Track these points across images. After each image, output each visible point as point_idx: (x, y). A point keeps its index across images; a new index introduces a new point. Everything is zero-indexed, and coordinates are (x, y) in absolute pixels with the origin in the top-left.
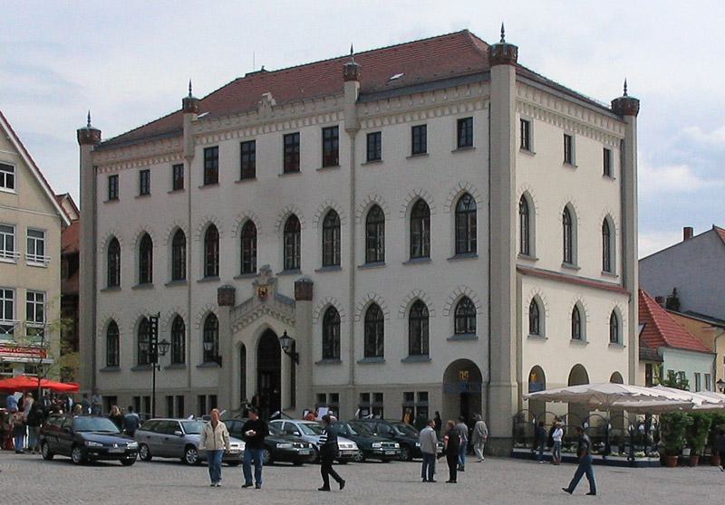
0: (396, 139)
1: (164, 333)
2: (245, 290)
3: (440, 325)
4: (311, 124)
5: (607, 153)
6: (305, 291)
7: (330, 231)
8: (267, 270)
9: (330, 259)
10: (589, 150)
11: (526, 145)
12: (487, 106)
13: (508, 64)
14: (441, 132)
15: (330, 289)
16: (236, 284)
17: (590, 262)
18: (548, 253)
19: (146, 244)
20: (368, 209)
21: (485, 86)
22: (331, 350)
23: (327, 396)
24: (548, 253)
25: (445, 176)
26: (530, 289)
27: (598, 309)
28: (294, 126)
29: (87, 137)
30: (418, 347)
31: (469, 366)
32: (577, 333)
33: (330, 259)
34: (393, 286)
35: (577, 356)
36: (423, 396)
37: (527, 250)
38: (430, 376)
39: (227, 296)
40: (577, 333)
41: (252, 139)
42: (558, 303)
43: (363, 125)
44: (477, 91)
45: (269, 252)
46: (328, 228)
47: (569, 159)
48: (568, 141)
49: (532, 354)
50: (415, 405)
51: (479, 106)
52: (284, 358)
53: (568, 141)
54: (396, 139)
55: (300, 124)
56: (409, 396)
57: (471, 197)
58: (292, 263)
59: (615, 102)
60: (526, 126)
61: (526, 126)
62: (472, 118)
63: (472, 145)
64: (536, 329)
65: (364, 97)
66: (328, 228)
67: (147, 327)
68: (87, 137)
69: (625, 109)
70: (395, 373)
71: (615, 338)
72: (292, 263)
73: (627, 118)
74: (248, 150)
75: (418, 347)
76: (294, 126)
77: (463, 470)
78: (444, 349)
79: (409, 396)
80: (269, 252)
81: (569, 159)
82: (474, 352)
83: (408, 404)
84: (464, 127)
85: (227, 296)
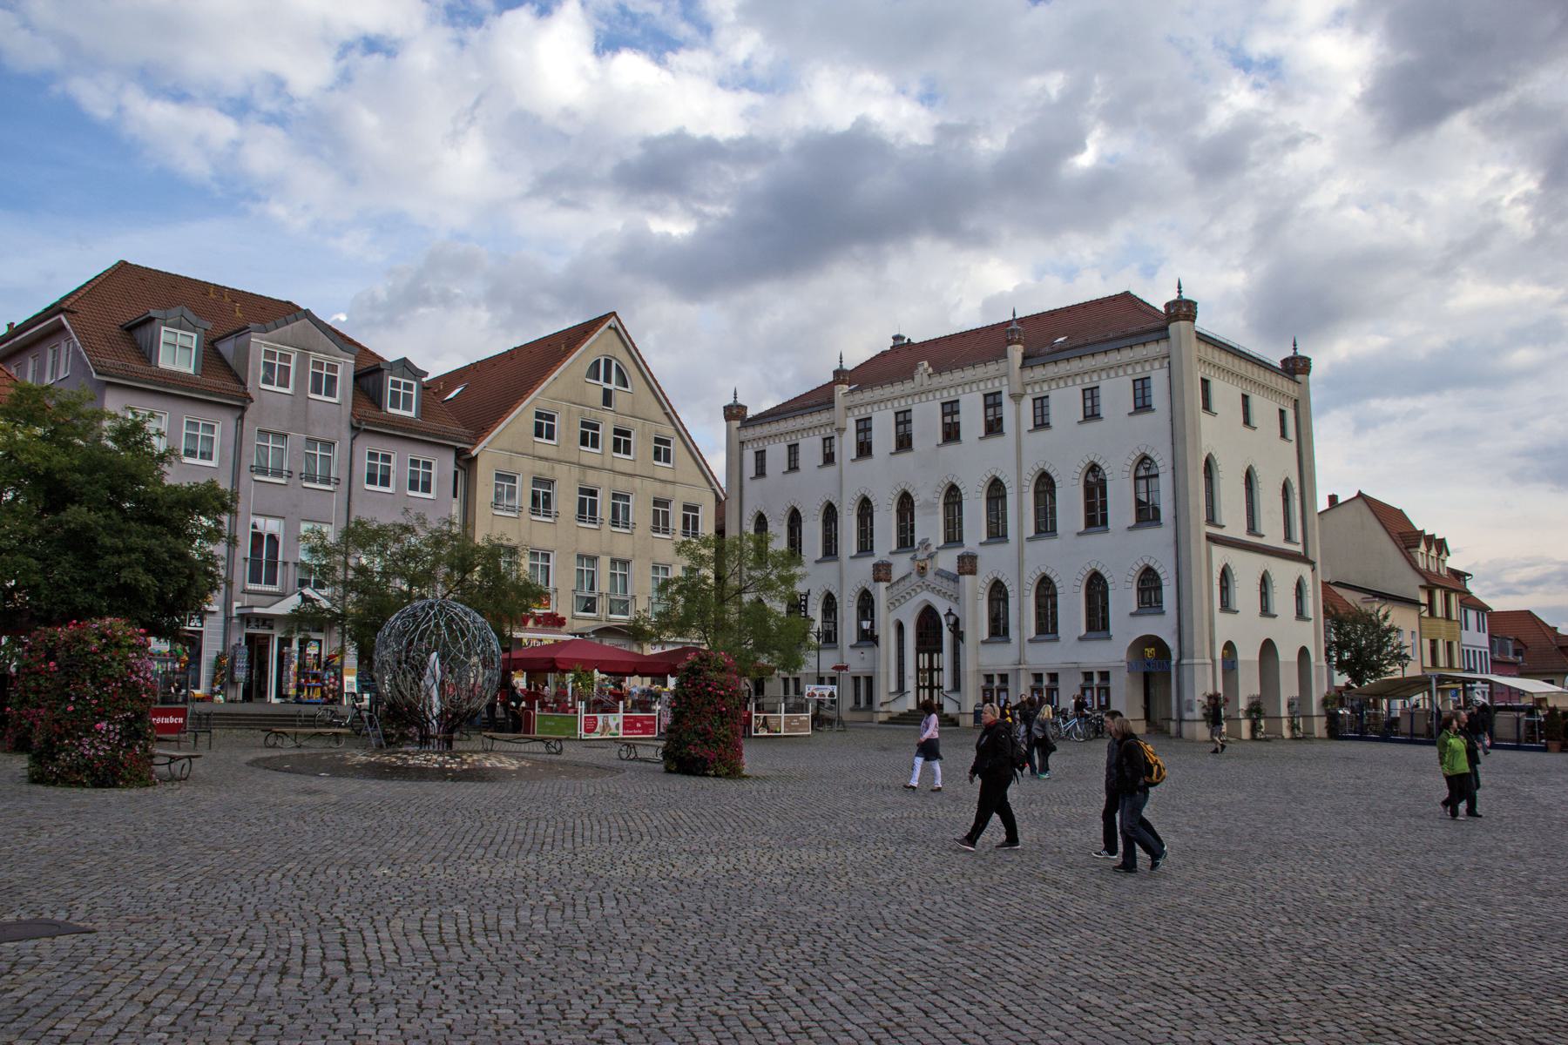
2: (902, 565)
3: (1123, 599)
5: (1282, 412)
6: (968, 564)
8: (925, 544)
9: (997, 532)
10: (1265, 409)
15: (995, 562)
16: (892, 559)
26: (1220, 555)
33: (997, 532)
34: (1069, 557)
35: (1267, 629)
37: (1211, 520)
38: (1111, 654)
39: (882, 572)
43: (1029, 390)
44: (1153, 349)
45: (929, 526)
53: (1245, 398)
58: (953, 536)
59: (1285, 362)
61: (1205, 382)
65: (1028, 360)
68: (734, 412)
72: (953, 536)
73: (1299, 377)
75: (1098, 622)
78: (1127, 624)
80: (929, 526)
82: (1161, 627)
84: (1142, 388)
85: (882, 572)
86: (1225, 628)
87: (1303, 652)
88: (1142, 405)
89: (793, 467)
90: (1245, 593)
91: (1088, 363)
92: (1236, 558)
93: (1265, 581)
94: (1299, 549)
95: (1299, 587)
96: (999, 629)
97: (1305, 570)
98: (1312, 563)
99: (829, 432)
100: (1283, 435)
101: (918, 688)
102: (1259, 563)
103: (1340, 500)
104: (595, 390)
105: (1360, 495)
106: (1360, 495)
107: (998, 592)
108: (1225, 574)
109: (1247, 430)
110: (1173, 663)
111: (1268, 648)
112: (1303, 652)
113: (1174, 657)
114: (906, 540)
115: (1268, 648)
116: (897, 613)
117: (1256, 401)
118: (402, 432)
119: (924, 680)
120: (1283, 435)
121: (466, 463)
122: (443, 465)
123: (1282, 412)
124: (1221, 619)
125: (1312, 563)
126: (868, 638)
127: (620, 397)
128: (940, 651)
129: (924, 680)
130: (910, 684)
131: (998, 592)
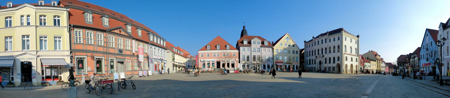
0: (332, 40)
1: (314, 63)
2: (318, 56)
3: (336, 59)
6: (323, 56)
9: (326, 53)
10: (354, 41)
11: (346, 40)
15: (326, 56)
17: (354, 52)
18: (348, 51)
19: (330, 59)
22: (326, 63)
24: (348, 51)
25: (337, 43)
26: (345, 55)
27: (354, 58)
29: (305, 42)
30: (334, 62)
31: (338, 64)
32: (352, 60)
33: (326, 53)
34: (332, 55)
35: (352, 63)
38: (335, 65)
39: (316, 57)
40: (352, 60)
42: (349, 57)
45: (320, 52)
49: (346, 62)
50: (334, 68)
54: (332, 40)
58: (322, 53)
64: (346, 60)
65: (329, 35)
67: (310, 60)
68: (305, 42)
69: (358, 36)
70: (332, 65)
71: (357, 61)
72: (322, 53)
74: (318, 42)
75: (334, 62)
77: (22, 36)
78: (337, 62)
80: (320, 52)
81: (351, 42)
82: (339, 62)
84: (339, 38)
85: (316, 57)
88: (339, 39)
89: (334, 40)
90: (349, 59)
93: (352, 58)
95: (357, 59)
96: (326, 63)
102: (351, 56)
104: (286, 41)
107: (326, 59)
108: (346, 57)
111: (352, 65)
114: (318, 54)
115: (352, 65)
116: (318, 61)
117: (352, 40)
118: (266, 47)
121: (273, 49)
122: (271, 49)
126: (315, 63)
127: (289, 41)
131: (326, 59)
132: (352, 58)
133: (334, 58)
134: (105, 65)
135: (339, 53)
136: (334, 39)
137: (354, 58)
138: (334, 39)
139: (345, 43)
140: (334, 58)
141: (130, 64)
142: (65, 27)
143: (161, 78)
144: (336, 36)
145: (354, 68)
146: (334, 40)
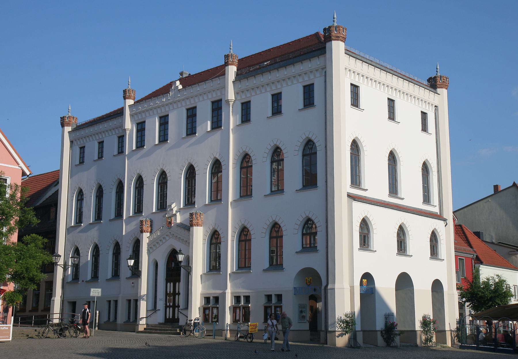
0: (261, 104)
3: (292, 240)
4: (204, 100)
5: (424, 115)
7: (243, 243)
11: (355, 102)
12: (324, 74)
13: (338, 40)
14: (293, 96)
17: (411, 192)
18: (375, 183)
20: (271, 226)
21: (322, 58)
23: (212, 298)
24: (375, 183)
25: (291, 130)
26: (361, 210)
27: (419, 229)
28: (192, 102)
30: (276, 263)
32: (402, 247)
35: (403, 265)
36: (279, 297)
37: (356, 179)
38: (284, 282)
40: (402, 247)
41: (166, 114)
46: (243, 241)
47: (392, 116)
48: (391, 102)
51: (318, 75)
52: (182, 270)
53: (391, 102)
55: (197, 100)
56: (269, 297)
57: (314, 143)
60: (355, 88)
61: (355, 88)
62: (313, 84)
63: (314, 104)
64: (365, 241)
66: (243, 241)
76: (192, 102)
78: (294, 261)
79: (269, 297)
81: (392, 116)
82: (311, 261)
83: (206, 306)
84: (309, 91)
86: (364, 262)
87: (437, 286)
88: (309, 100)
89: (277, 110)
90: (384, 236)
91: (275, 75)
92: (412, 222)
93: (401, 231)
94: (436, 210)
95: (434, 238)
97: (438, 225)
98: (445, 220)
99: (120, 133)
100: (425, 128)
101: (166, 307)
103: (501, 188)
105: (514, 184)
106: (514, 184)
108: (365, 224)
109: (391, 123)
110: (323, 288)
111: (404, 282)
112: (437, 286)
113: (324, 284)
115: (404, 282)
119: (170, 302)
120: (425, 128)
123: (424, 115)
124: (360, 255)
125: (445, 220)
128: (179, 281)
129: (170, 302)
130: (161, 305)
132: (401, 231)
133: (275, 232)
134: (179, 294)
135: (313, 195)
136: (277, 98)
137: (419, 229)
138: (277, 98)
139: (348, 124)
140: (275, 232)
141: (198, 289)
142: (247, 170)
143: (147, 347)
144: (290, 85)
145: (423, 307)
146: (277, 110)
